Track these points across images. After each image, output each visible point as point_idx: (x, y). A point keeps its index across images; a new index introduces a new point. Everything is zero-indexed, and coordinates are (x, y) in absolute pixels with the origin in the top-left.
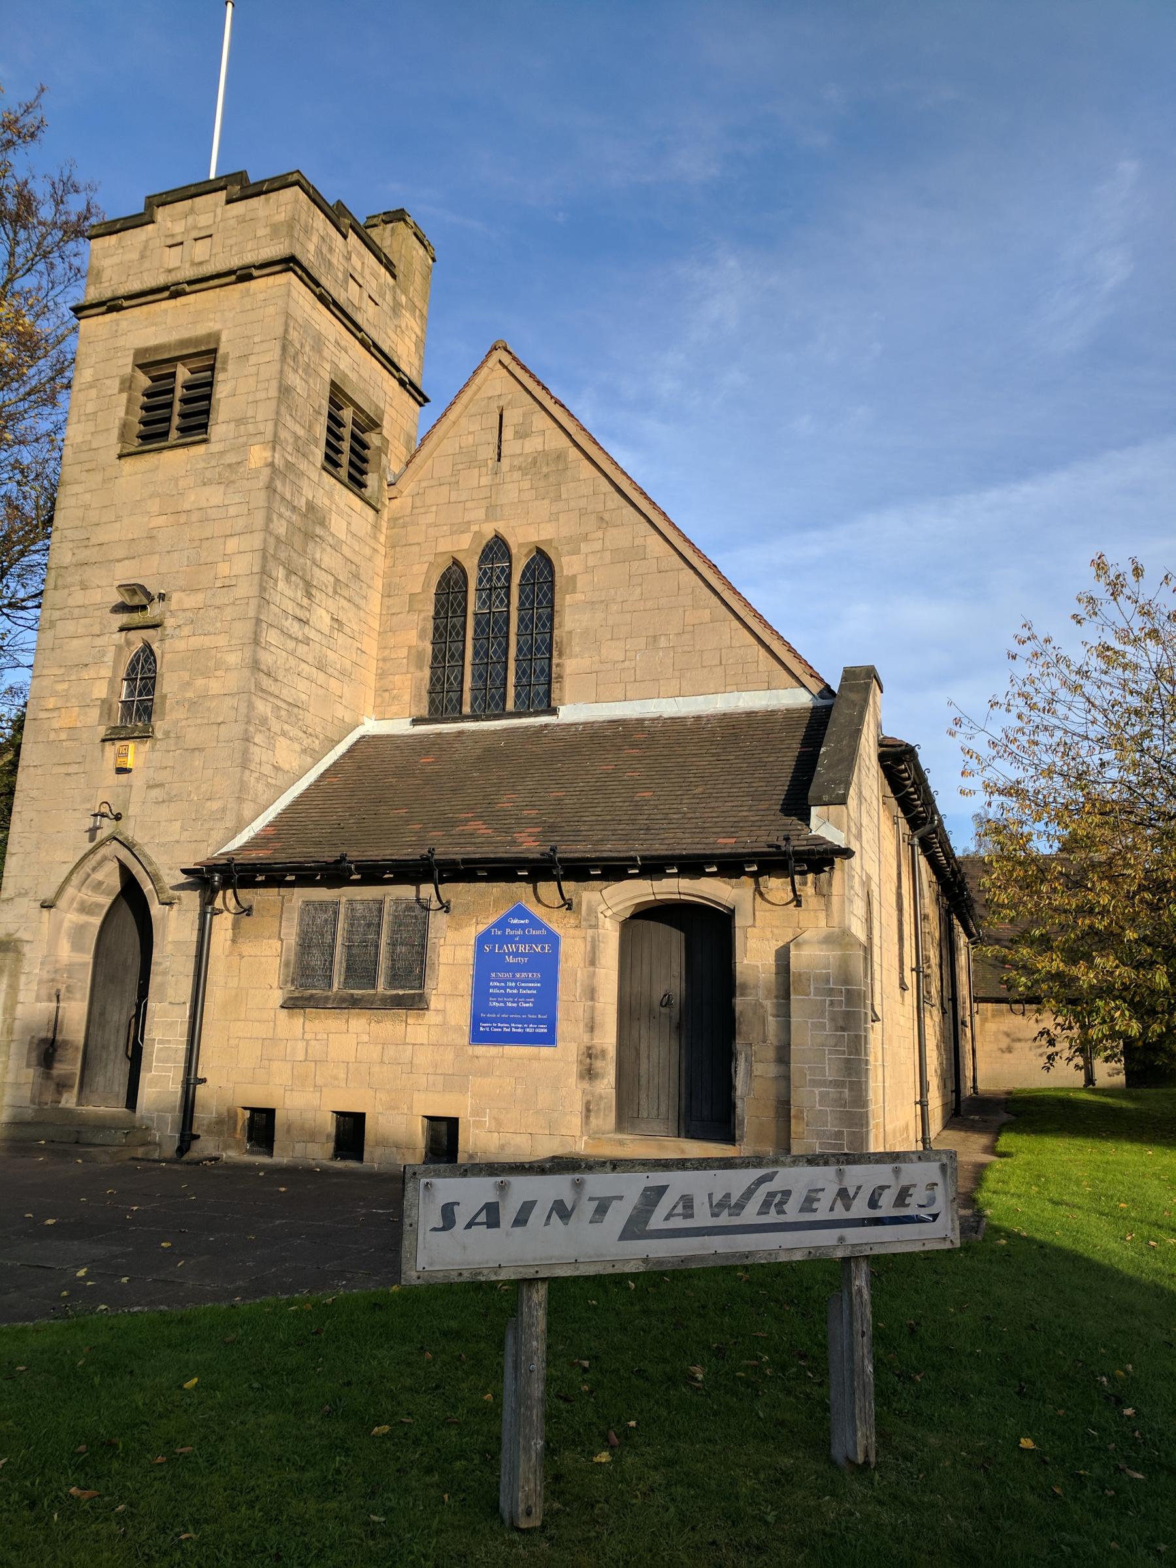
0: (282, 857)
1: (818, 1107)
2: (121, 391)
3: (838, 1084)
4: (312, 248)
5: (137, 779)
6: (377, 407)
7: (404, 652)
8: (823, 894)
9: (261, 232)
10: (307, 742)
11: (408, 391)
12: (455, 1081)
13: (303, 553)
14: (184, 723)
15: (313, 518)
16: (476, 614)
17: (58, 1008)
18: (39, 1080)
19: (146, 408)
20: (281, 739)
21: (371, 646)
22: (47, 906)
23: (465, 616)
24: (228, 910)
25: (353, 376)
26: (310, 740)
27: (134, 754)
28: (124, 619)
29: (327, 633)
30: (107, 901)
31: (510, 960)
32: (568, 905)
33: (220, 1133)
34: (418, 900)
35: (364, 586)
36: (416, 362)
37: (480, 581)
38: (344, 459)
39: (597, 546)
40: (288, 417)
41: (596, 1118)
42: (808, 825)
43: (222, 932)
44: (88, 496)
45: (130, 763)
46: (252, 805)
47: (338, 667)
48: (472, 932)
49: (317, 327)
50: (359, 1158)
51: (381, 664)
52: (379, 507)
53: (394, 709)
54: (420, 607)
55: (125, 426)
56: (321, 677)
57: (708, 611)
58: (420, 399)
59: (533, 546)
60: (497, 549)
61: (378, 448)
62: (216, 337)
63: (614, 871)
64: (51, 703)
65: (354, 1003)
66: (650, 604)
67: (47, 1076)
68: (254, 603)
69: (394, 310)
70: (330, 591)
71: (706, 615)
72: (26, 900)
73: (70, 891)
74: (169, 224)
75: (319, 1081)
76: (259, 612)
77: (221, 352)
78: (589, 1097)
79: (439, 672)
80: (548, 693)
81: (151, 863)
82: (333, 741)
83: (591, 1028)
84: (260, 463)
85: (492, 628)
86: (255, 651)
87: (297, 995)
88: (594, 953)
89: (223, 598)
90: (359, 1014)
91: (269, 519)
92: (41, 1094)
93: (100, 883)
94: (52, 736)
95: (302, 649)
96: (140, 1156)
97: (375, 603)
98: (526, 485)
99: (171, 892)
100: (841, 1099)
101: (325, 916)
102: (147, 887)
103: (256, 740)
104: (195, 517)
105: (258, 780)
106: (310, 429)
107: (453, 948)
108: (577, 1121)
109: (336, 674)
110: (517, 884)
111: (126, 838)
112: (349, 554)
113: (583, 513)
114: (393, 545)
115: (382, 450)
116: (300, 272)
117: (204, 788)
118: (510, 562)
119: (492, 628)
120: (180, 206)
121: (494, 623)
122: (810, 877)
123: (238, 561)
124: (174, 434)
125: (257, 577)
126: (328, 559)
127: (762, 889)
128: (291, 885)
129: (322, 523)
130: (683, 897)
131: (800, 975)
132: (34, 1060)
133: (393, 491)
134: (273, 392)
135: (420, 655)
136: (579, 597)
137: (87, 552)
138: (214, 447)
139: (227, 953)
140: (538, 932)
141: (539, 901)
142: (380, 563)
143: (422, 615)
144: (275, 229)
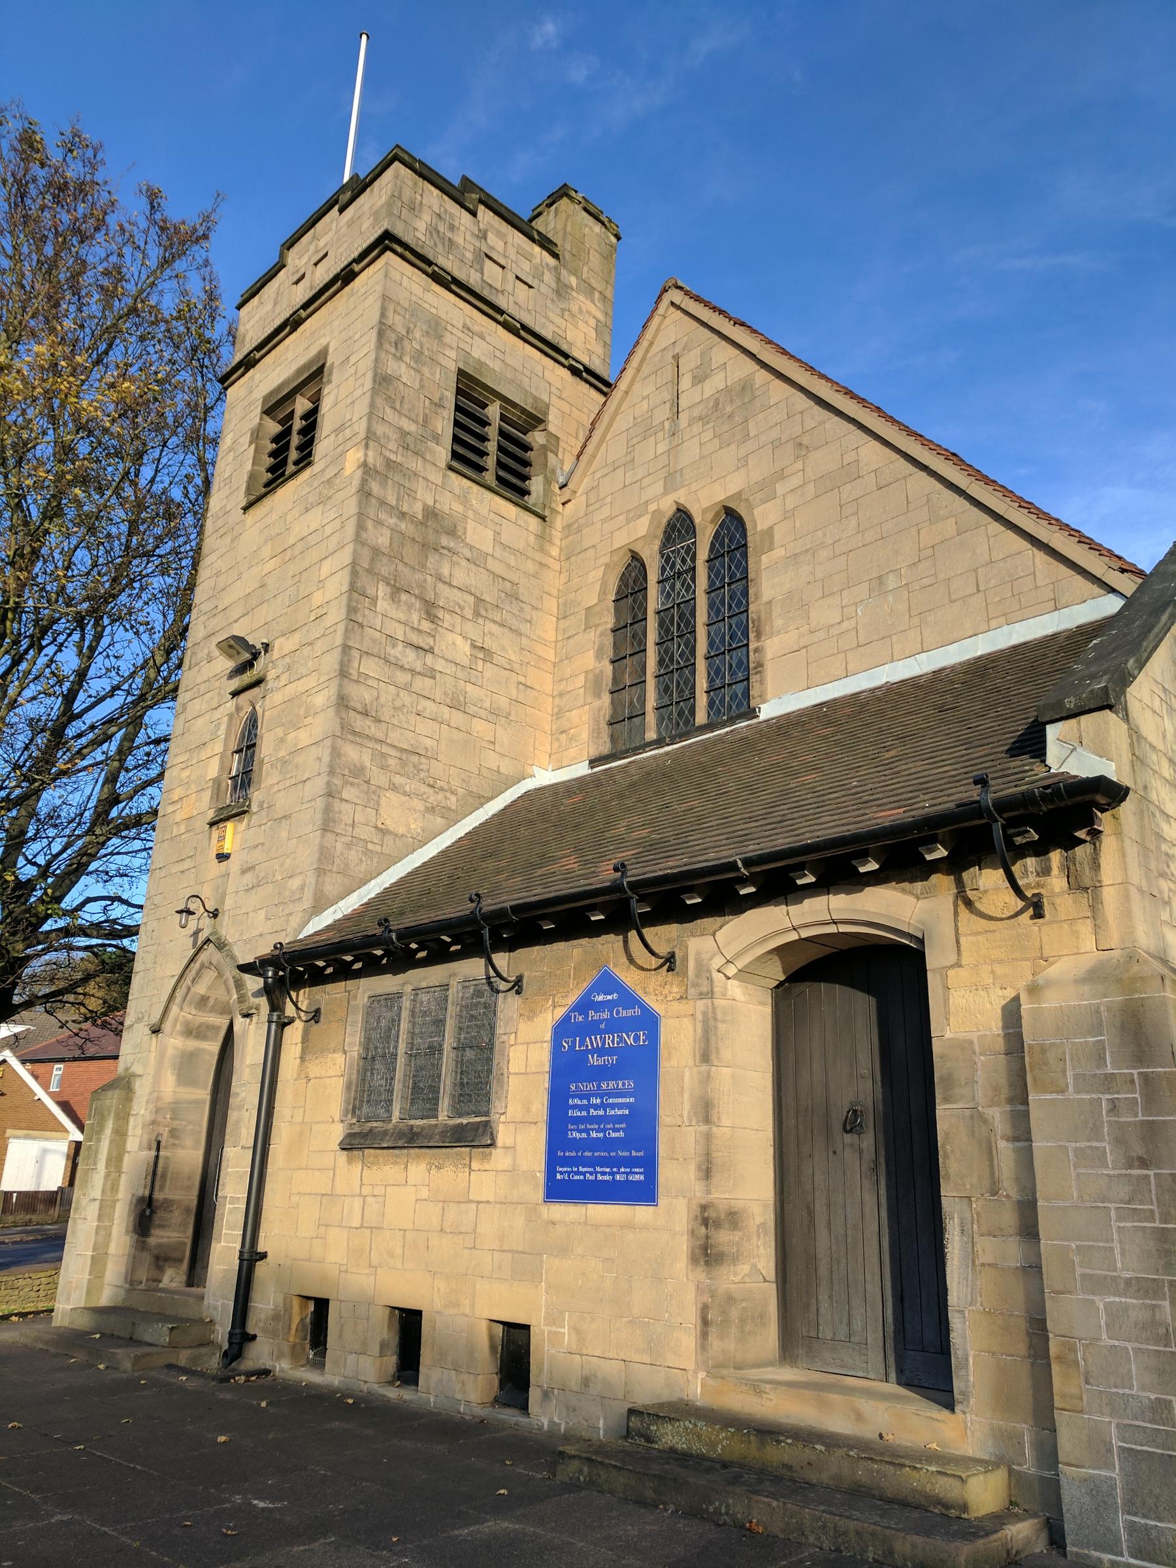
1: (1106, 1340)
3: (1147, 1289)
5: (233, 865)
6: (535, 399)
8: (1084, 886)
10: (433, 799)
11: (587, 381)
12: (525, 1265)
14: (276, 788)
17: (157, 1157)
22: (156, 1031)
25: (496, 365)
27: (232, 836)
29: (466, 663)
31: (594, 1060)
35: (527, 608)
37: (663, 569)
39: (796, 481)
40: (388, 410)
41: (722, 1337)
42: (1044, 761)
44: (219, 561)
45: (227, 848)
46: (340, 878)
47: (487, 705)
49: (434, 311)
51: (557, 701)
52: (547, 513)
53: (572, 752)
54: (597, 621)
55: (252, 477)
56: (457, 718)
57: (953, 520)
61: (544, 448)
63: (717, 894)
69: (558, 292)
70: (469, 613)
71: (950, 527)
80: (747, 694)
85: (677, 624)
86: (341, 686)
87: (356, 1130)
90: (418, 1157)
91: (361, 527)
95: (421, 684)
98: (708, 435)
100: (1154, 1323)
103: (345, 795)
108: (688, 1341)
109: (483, 713)
113: (776, 445)
116: (399, 249)
119: (677, 624)
122: (1056, 857)
126: (462, 574)
127: (970, 894)
128: (358, 975)
129: (452, 532)
130: (843, 929)
131: (1044, 1050)
132: (131, 1228)
136: (779, 552)
137: (214, 621)
139: (295, 1076)
140: (630, 1013)
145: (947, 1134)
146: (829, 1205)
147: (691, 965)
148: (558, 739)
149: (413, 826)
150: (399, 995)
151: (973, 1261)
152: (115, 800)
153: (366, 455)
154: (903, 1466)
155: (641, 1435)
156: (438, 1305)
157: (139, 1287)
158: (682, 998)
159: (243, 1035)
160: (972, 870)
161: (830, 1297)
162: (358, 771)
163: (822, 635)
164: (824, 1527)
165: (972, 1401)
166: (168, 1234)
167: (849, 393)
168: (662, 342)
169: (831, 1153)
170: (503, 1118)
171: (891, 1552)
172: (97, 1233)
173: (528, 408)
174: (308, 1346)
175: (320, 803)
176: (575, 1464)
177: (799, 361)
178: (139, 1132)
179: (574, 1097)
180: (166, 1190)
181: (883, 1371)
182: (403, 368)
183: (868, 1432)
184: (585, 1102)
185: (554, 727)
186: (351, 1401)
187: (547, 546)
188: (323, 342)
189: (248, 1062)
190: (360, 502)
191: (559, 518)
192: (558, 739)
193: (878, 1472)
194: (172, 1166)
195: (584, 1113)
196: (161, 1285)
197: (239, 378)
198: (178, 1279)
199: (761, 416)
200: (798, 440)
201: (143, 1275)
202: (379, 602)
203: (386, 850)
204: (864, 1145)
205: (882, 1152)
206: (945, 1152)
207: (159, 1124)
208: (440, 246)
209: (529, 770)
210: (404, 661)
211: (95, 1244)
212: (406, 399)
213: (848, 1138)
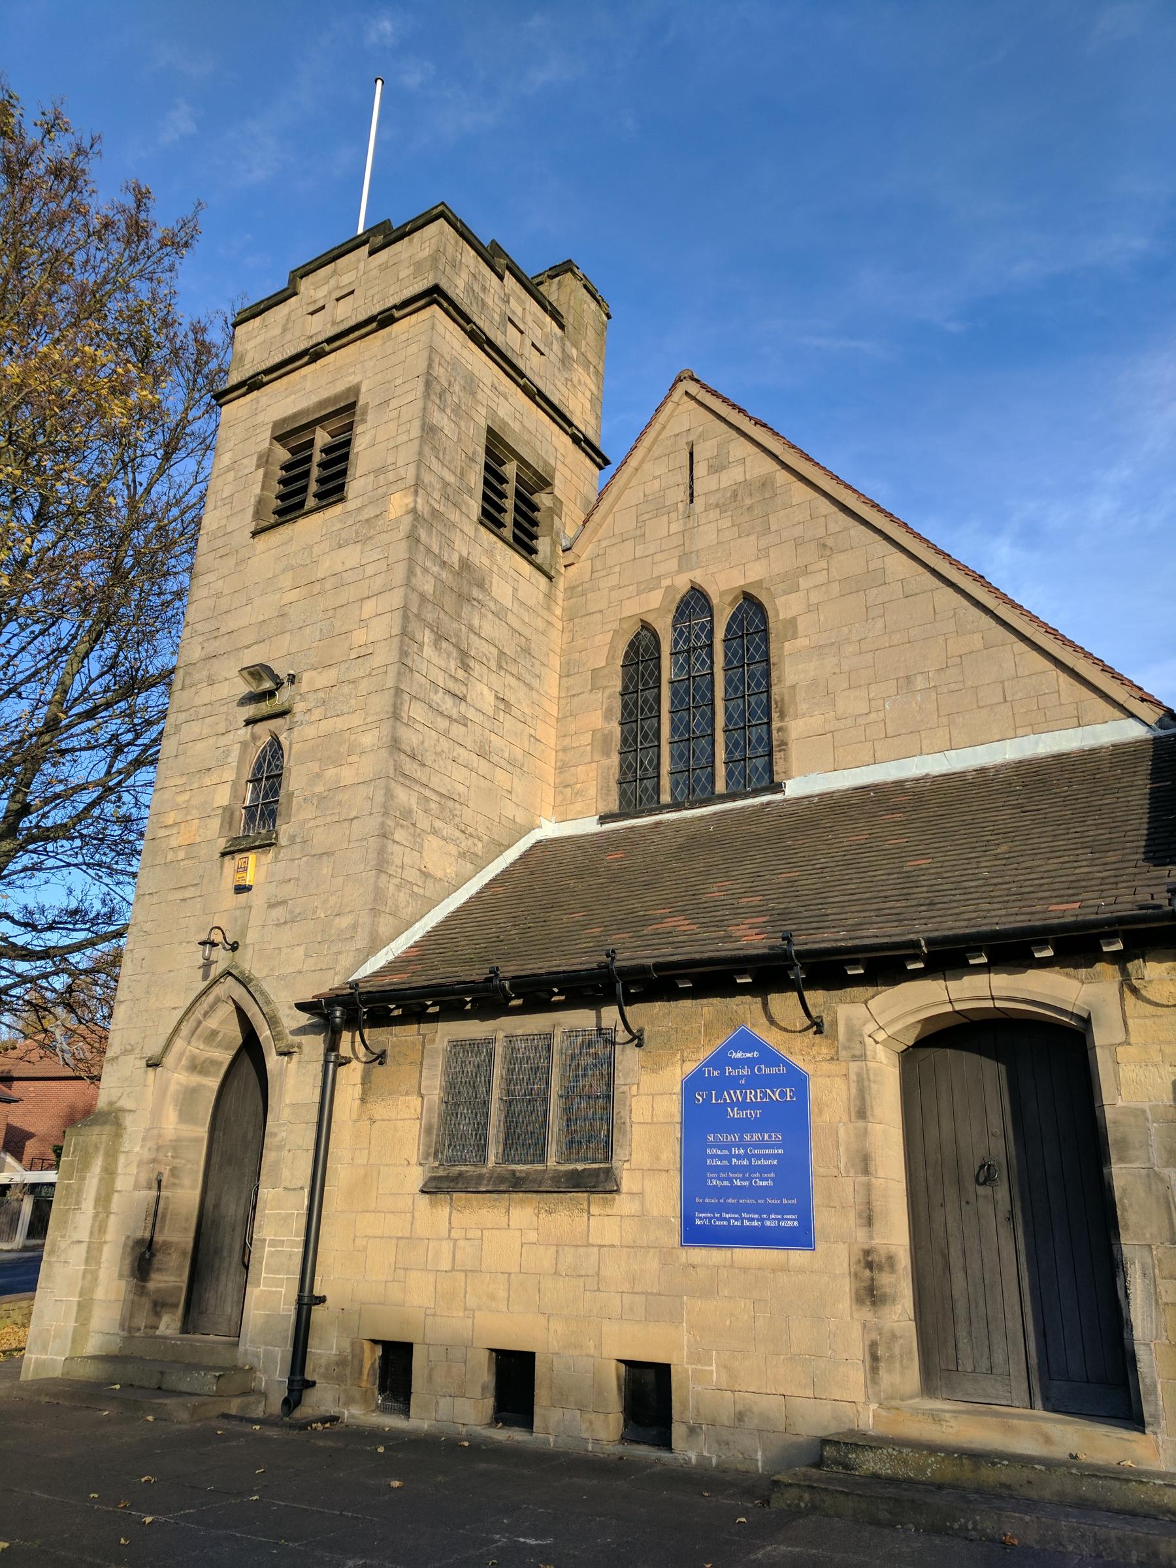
0: (420, 981)
4: (461, 283)
5: (256, 898)
7: (588, 738)
10: (466, 844)
11: (584, 450)
13: (457, 617)
14: (312, 823)
15: (468, 581)
16: (671, 683)
17: (158, 1197)
18: (131, 1296)
19: (282, 482)
20: (431, 837)
21: (549, 735)
22: (153, 1064)
23: (659, 687)
24: (357, 1058)
25: (516, 426)
26: (470, 842)
27: (255, 868)
28: (250, 711)
29: (491, 713)
30: (226, 1057)
31: (734, 1113)
32: (817, 1026)
33: (340, 1379)
34: (600, 1030)
35: (537, 663)
36: (593, 422)
37: (676, 643)
38: (508, 518)
39: (821, 578)
40: (434, 460)
41: (889, 1371)
43: (350, 1088)
44: (220, 583)
46: (391, 919)
47: (506, 755)
48: (675, 1074)
49: (469, 367)
50: (528, 1424)
51: (561, 755)
52: (553, 573)
53: (578, 806)
54: (605, 683)
55: (260, 502)
56: (483, 766)
57: (978, 636)
58: (599, 460)
59: (738, 591)
60: (695, 602)
61: (551, 510)
63: (885, 967)
64: (170, 818)
65: (516, 1185)
66: (897, 638)
67: (141, 1291)
68: (393, 671)
69: (563, 362)
70: (493, 665)
71: (977, 641)
72: (132, 1057)
73: (179, 1044)
74: (312, 292)
75: (471, 1301)
76: (399, 680)
78: (874, 1336)
79: (630, 757)
81: (268, 1002)
82: (500, 845)
83: (868, 1219)
85: (694, 696)
86: (394, 728)
87: (441, 1173)
88: (863, 1099)
89: (358, 671)
90: (522, 1201)
91: (411, 572)
92: (132, 1316)
93: (214, 1033)
94: (170, 856)
95: (457, 730)
96: (234, 1412)
97: (551, 683)
98: (726, 523)
99: (290, 1037)
101: (476, 1060)
102: (264, 1033)
103: (397, 837)
105: (399, 887)
106: (462, 476)
107: (651, 1099)
108: (857, 1375)
109: (503, 763)
110: (739, 999)
111: (242, 973)
112: (516, 624)
113: (799, 542)
114: (571, 617)
115: (556, 509)
116: (445, 305)
117: (333, 900)
118: (712, 616)
119: (694, 696)
120: (322, 272)
121: (700, 688)
123: (376, 626)
124: (311, 502)
125: (396, 640)
126: (489, 627)
128: (435, 1018)
129: (481, 585)
130: (999, 1004)
132: (127, 1270)
133: (570, 557)
134: (416, 432)
136: (801, 642)
137: (216, 643)
138: (351, 504)
139: (354, 1117)
140: (774, 1070)
141: (772, 1021)
142: (557, 639)
143: (608, 692)
144: (418, 266)
145: (1124, 1190)
146: (964, 1252)
147: (841, 1029)
148: (562, 793)
149: (448, 871)
150: (491, 1042)
151: (1157, 1301)
152: (26, 810)
153: (415, 501)
154: (1129, 1481)
155: (837, 1463)
156: (555, 1346)
157: (137, 1334)
158: (832, 1059)
159: (280, 1074)
160: (1136, 962)
161: (970, 1333)
162: (407, 814)
163: (849, 722)
164: (1083, 1536)
165: (1163, 1423)
166: (166, 1278)
167: (875, 506)
168: (675, 428)
169: (963, 1203)
170: (626, 1165)
171: (1155, 1554)
172: (84, 1278)
173: (540, 470)
174: (376, 1392)
175: (373, 843)
176: (794, 1492)
177: (824, 468)
178: (134, 1169)
179: (711, 1147)
180: (166, 1231)
181: (1027, 1399)
182: (446, 421)
183: (1059, 1452)
184: (725, 1152)
185: (558, 780)
186: (466, 1444)
187: (553, 606)
188: (352, 380)
189: (288, 1101)
190: (410, 549)
191: (562, 579)
192: (562, 793)
193: (1102, 1487)
194: (171, 1206)
195: (725, 1163)
196: (158, 1333)
197: (238, 397)
198: (173, 1326)
199: (782, 513)
200: (822, 541)
201: (141, 1321)
202: (426, 648)
203: (428, 894)
204: (999, 1197)
205: (1018, 1204)
206: (1123, 1205)
207: (160, 1163)
208: (475, 305)
209: (537, 822)
210: (443, 708)
211: (82, 1289)
212: (447, 451)
213: (981, 1190)
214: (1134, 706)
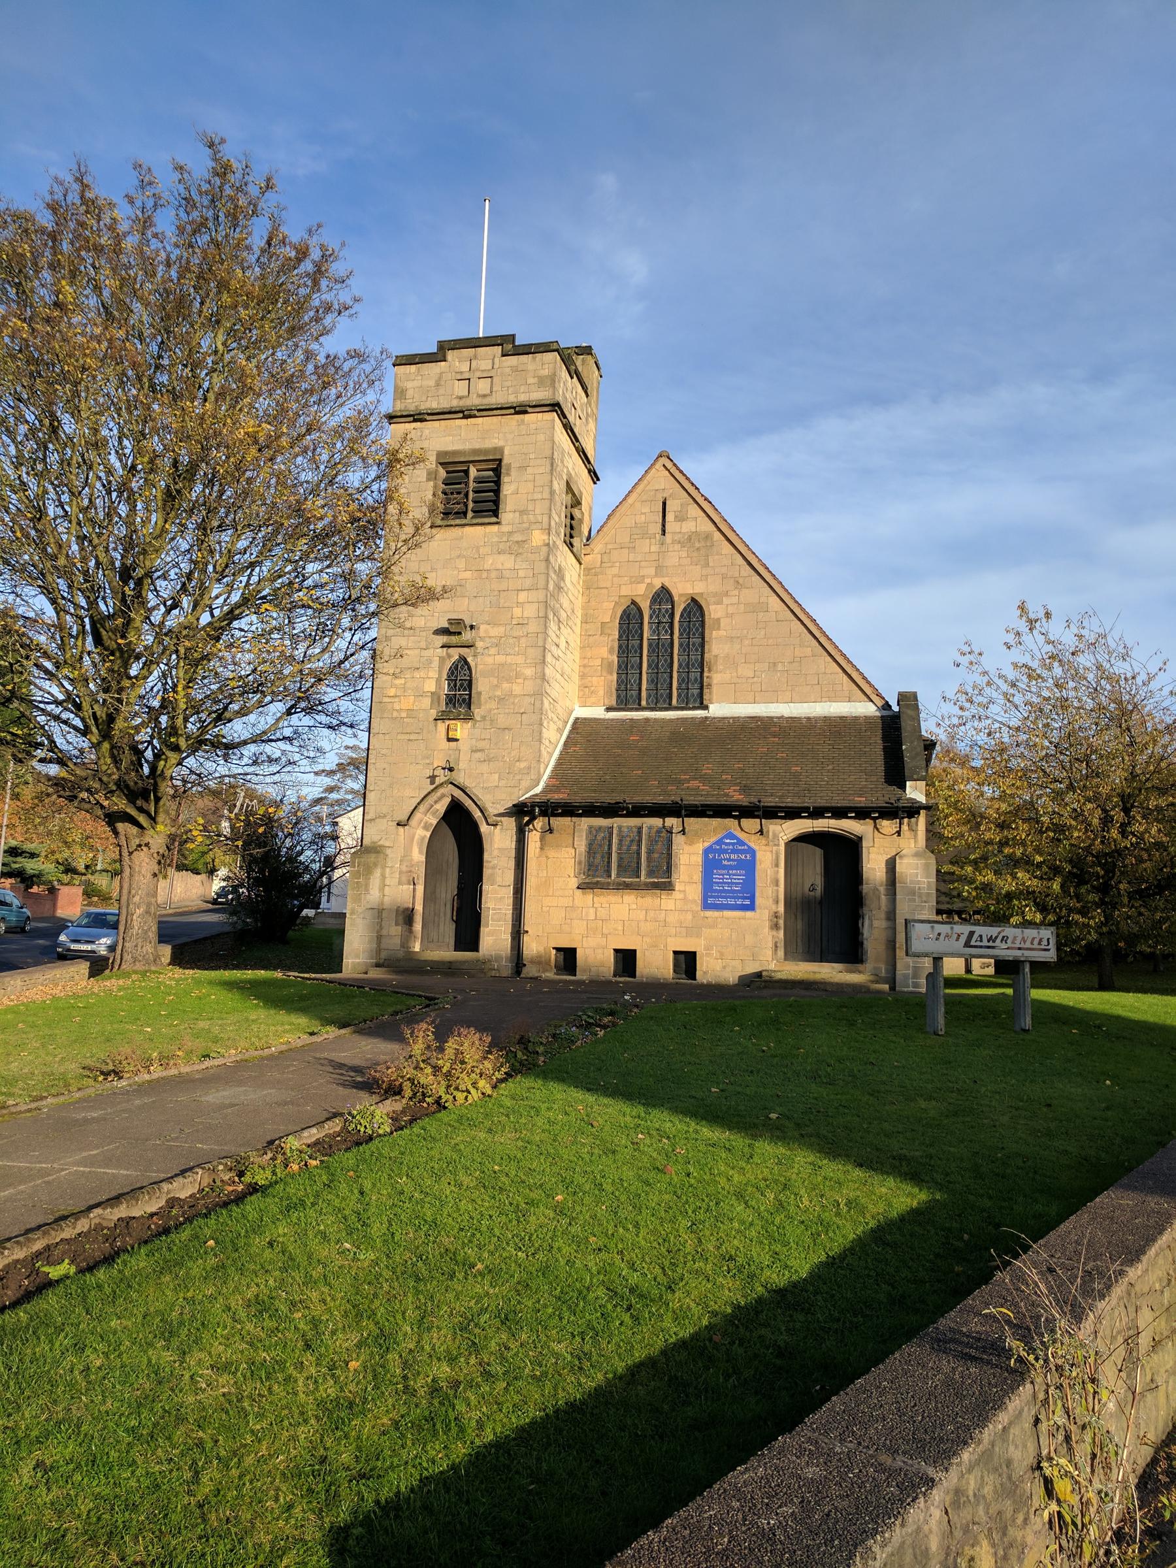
2: (428, 480)
7: (598, 662)
9: (531, 380)
12: (692, 931)
27: (461, 730)
28: (444, 639)
30: (435, 822)
31: (725, 863)
37: (651, 617)
39: (735, 600)
48: (700, 847)
53: (593, 700)
60: (663, 596)
62: (500, 450)
63: (792, 813)
64: (392, 692)
65: (627, 887)
71: (808, 651)
73: (418, 816)
77: (504, 462)
84: (540, 543)
85: (661, 649)
89: (518, 632)
94: (395, 714)
98: (684, 554)
104: (494, 574)
107: (690, 853)
108: (770, 952)
119: (661, 649)
121: (661, 645)
124: (470, 514)
135: (610, 664)
136: (722, 633)
138: (505, 528)
214: (874, 697)
